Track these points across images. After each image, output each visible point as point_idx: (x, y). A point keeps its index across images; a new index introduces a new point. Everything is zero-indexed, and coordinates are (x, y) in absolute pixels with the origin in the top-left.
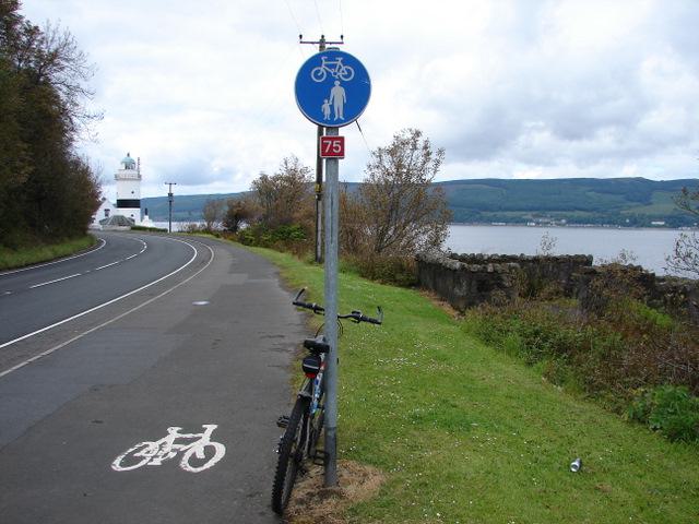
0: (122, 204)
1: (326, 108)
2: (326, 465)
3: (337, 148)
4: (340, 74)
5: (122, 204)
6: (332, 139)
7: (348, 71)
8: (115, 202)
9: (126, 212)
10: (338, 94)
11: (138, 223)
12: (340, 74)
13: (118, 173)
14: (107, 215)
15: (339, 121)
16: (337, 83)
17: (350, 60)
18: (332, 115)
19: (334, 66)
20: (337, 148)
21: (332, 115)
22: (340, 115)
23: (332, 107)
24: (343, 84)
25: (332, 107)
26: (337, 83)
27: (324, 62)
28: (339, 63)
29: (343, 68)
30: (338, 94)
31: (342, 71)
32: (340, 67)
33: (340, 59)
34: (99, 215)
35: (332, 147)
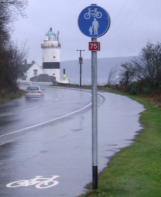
0: (46, 65)
1: (91, 30)
2: (127, 82)
3: (95, 47)
4: (96, 15)
5: (46, 65)
6: (94, 43)
7: (89, 16)
8: (41, 65)
9: (50, 72)
10: (95, 24)
11: (58, 80)
12: (96, 15)
13: (43, 43)
14: (35, 74)
15: (96, 35)
16: (95, 19)
17: (100, 9)
18: (93, 33)
19: (93, 12)
20: (95, 47)
21: (93, 33)
22: (96, 33)
23: (93, 29)
24: (97, 20)
25: (93, 29)
26: (95, 19)
27: (90, 11)
28: (96, 11)
29: (98, 13)
30: (95, 24)
31: (97, 14)
32: (96, 13)
33: (96, 9)
34: (30, 74)
35: (93, 47)
